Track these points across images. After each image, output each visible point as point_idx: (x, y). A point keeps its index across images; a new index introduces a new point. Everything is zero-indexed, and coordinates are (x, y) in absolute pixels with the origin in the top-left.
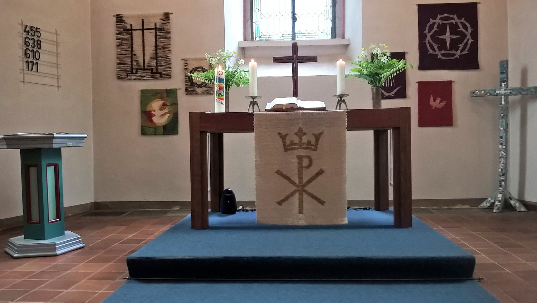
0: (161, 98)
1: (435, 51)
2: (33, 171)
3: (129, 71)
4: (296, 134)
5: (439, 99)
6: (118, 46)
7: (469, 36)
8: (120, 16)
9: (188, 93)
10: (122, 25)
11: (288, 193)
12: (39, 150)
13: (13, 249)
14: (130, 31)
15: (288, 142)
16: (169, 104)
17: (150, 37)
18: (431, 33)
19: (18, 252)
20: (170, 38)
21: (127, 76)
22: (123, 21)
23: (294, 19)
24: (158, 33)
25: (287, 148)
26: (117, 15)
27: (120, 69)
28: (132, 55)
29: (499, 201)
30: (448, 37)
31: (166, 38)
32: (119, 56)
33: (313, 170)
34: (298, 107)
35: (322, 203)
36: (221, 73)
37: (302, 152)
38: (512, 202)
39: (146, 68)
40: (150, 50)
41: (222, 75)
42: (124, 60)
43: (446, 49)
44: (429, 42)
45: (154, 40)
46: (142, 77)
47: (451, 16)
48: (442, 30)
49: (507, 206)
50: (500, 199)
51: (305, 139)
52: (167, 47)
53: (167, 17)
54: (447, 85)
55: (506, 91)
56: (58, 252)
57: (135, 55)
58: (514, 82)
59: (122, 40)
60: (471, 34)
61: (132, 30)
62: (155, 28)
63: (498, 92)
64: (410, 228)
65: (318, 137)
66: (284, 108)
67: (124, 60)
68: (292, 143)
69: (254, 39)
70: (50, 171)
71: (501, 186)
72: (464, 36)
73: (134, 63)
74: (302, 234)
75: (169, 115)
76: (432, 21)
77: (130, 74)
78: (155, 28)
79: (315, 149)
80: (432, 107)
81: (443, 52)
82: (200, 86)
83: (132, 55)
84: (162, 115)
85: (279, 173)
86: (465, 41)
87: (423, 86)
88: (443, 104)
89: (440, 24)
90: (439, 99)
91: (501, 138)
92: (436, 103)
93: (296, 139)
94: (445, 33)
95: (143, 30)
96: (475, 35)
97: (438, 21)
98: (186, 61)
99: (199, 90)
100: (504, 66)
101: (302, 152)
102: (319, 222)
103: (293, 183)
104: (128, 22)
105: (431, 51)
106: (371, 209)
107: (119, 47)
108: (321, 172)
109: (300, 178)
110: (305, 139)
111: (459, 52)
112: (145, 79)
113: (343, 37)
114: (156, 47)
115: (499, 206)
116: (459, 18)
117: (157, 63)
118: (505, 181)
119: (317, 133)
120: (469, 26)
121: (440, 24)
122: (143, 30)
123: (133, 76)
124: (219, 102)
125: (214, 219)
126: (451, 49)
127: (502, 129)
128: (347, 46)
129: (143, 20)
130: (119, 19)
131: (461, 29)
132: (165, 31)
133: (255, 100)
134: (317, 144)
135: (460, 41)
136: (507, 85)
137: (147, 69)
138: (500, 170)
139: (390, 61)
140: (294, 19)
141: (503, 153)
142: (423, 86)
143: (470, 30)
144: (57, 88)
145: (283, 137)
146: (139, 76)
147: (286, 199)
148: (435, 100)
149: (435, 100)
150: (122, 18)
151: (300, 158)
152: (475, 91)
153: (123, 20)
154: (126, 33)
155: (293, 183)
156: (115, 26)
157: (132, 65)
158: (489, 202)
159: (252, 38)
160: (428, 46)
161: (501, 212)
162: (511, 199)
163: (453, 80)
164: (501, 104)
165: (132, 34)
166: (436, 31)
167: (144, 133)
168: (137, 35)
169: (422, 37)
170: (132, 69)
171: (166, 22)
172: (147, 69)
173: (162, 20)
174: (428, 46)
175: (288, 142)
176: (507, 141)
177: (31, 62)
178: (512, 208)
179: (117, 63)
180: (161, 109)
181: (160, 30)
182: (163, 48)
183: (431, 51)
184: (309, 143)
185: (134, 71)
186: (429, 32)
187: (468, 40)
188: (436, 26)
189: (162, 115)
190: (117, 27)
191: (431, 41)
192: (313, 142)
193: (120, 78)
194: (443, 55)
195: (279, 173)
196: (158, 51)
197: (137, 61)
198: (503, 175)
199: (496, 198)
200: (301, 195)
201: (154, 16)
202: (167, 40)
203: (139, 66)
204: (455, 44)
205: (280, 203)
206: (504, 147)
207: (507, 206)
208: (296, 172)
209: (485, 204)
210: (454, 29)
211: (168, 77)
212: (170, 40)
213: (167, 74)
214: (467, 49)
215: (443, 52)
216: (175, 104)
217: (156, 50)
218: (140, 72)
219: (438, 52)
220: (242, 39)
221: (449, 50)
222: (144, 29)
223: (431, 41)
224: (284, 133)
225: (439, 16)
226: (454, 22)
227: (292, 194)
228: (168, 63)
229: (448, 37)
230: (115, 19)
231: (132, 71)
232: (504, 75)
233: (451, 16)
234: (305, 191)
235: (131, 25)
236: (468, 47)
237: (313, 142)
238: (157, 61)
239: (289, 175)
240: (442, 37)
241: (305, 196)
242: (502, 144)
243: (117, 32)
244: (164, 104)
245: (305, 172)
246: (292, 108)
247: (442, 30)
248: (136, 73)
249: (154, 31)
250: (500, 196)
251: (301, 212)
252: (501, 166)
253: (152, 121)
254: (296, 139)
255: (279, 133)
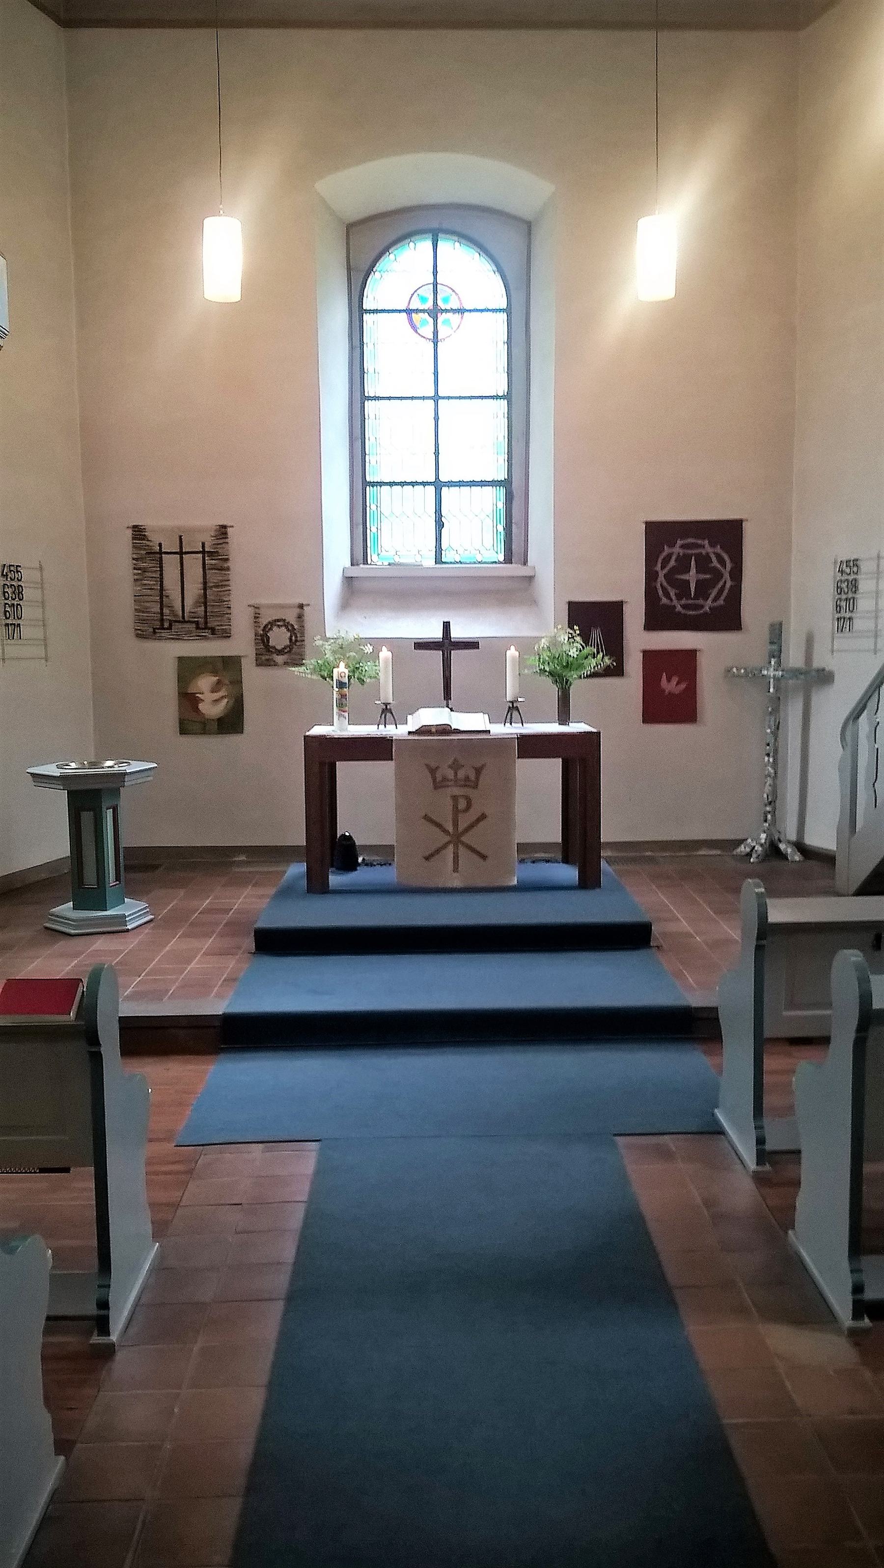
0: (214, 672)
1: (671, 600)
2: (87, 817)
3: (157, 624)
4: (450, 767)
5: (675, 680)
6: (136, 580)
7: (727, 576)
8: (141, 528)
9: (260, 663)
10: (143, 543)
11: (439, 845)
12: (98, 791)
13: (71, 925)
14: (158, 556)
15: (439, 778)
16: (227, 682)
17: (194, 566)
18: (665, 571)
19: (76, 927)
20: (228, 569)
21: (155, 632)
22: (144, 538)
23: (440, 525)
24: (207, 560)
25: (439, 785)
26: (135, 527)
27: (141, 621)
28: (161, 598)
29: (762, 845)
30: (692, 576)
31: (221, 569)
32: (138, 598)
33: (472, 815)
34: (453, 728)
35: (484, 857)
36: (343, 675)
37: (457, 791)
38: (782, 846)
39: (186, 619)
40: (193, 589)
41: (345, 677)
42: (148, 604)
43: (688, 596)
44: (661, 585)
45: (202, 572)
46: (179, 635)
47: (699, 542)
48: (683, 565)
49: (773, 851)
50: (763, 841)
51: (461, 774)
52: (223, 585)
53: (222, 532)
54: (689, 657)
55: (777, 673)
56: (129, 927)
57: (167, 596)
58: (794, 658)
59: (144, 570)
60: (730, 573)
61: (161, 553)
62: (203, 552)
63: (765, 672)
64: (598, 890)
65: (478, 771)
66: (434, 730)
67: (148, 604)
68: (445, 779)
69: (369, 562)
70: (110, 813)
71: (766, 821)
72: (718, 576)
73: (166, 611)
74: (458, 898)
75: (226, 700)
76: (667, 550)
77: (158, 629)
78: (203, 552)
79: (476, 786)
80: (664, 691)
81: (683, 602)
82: (280, 652)
83: (161, 598)
84: (216, 701)
85: (426, 818)
86: (721, 584)
87: (650, 657)
88: (683, 686)
89: (681, 554)
90: (675, 680)
91: (768, 745)
92: (670, 686)
93: (450, 774)
94: (687, 570)
95: (181, 553)
96: (737, 574)
97: (677, 550)
98: (257, 610)
99: (280, 659)
100: (776, 633)
101: (457, 791)
102: (480, 883)
103: (445, 831)
104: (155, 539)
105: (664, 600)
106: (557, 862)
107: (139, 583)
108: (483, 817)
109: (455, 824)
110: (461, 774)
111: (709, 602)
112: (187, 638)
113: (525, 563)
114: (205, 583)
115: (759, 852)
116: (712, 545)
117: (206, 612)
118: (773, 813)
119: (479, 765)
120: (726, 557)
121: (681, 554)
122: (181, 553)
123: (165, 633)
124: (340, 716)
125: (335, 879)
126: (696, 597)
127: (769, 731)
128: (530, 579)
129: (180, 537)
130: (138, 533)
131: (715, 563)
132: (220, 557)
133: (388, 707)
134: (477, 778)
135: (711, 584)
136: (779, 663)
137: (189, 622)
138: (765, 796)
139: (583, 648)
140: (440, 525)
141: (770, 769)
142: (650, 657)
143: (729, 565)
144: (43, 661)
145: (433, 771)
146: (175, 633)
147: (438, 851)
148: (669, 680)
149: (669, 680)
150: (142, 532)
151: (455, 798)
152: (732, 668)
153: (145, 535)
154: (151, 559)
155: (445, 831)
156: (131, 545)
157: (162, 614)
158: (748, 845)
159: (365, 562)
160: (660, 592)
161: (763, 861)
162: (780, 841)
163: (698, 647)
164: (769, 692)
165: (161, 558)
166: (673, 567)
167: (184, 729)
168: (171, 564)
169: (651, 576)
170: (162, 620)
171: (221, 541)
172: (189, 622)
173: (215, 538)
174: (660, 592)
175: (439, 778)
176: (776, 751)
177: (11, 624)
178: (783, 856)
179: (136, 610)
180: (213, 691)
181: (211, 554)
182: (217, 587)
183: (664, 600)
184: (467, 778)
185: (166, 625)
186: (663, 568)
187: (725, 582)
188: (674, 558)
189: (216, 701)
190: (134, 547)
191: (665, 584)
192: (472, 777)
193: (140, 635)
194: (684, 607)
195: (426, 818)
196: (208, 591)
197: (170, 607)
198: (770, 803)
199: (757, 839)
200: (456, 847)
201: (201, 530)
202: (223, 572)
203: (176, 615)
204: (703, 589)
205: (427, 858)
206: (771, 760)
207: (773, 851)
208: (450, 817)
209: (743, 849)
210: (703, 563)
211: (226, 635)
212: (229, 572)
213: (225, 631)
214: (722, 598)
215: (683, 602)
216: (238, 682)
217: (205, 589)
218: (176, 626)
219: (675, 602)
220: (348, 564)
221: (694, 599)
222: (183, 552)
223: (665, 584)
224: (433, 765)
225: (679, 542)
226: (704, 552)
227: (445, 846)
228: (224, 609)
229: (692, 576)
230: (129, 533)
231: (162, 625)
232: (775, 647)
233: (699, 542)
234: (463, 843)
235: (160, 545)
236: (726, 591)
237: (472, 777)
238: (206, 608)
239: (438, 820)
240: (685, 577)
241: (462, 850)
242: (768, 755)
243: (135, 556)
244: (219, 682)
245: (461, 816)
246: (445, 730)
247: (683, 565)
248: (170, 628)
249: (200, 555)
250: (763, 836)
251: (456, 869)
252: (768, 789)
253: (197, 710)
254: (450, 774)
255: (427, 766)
